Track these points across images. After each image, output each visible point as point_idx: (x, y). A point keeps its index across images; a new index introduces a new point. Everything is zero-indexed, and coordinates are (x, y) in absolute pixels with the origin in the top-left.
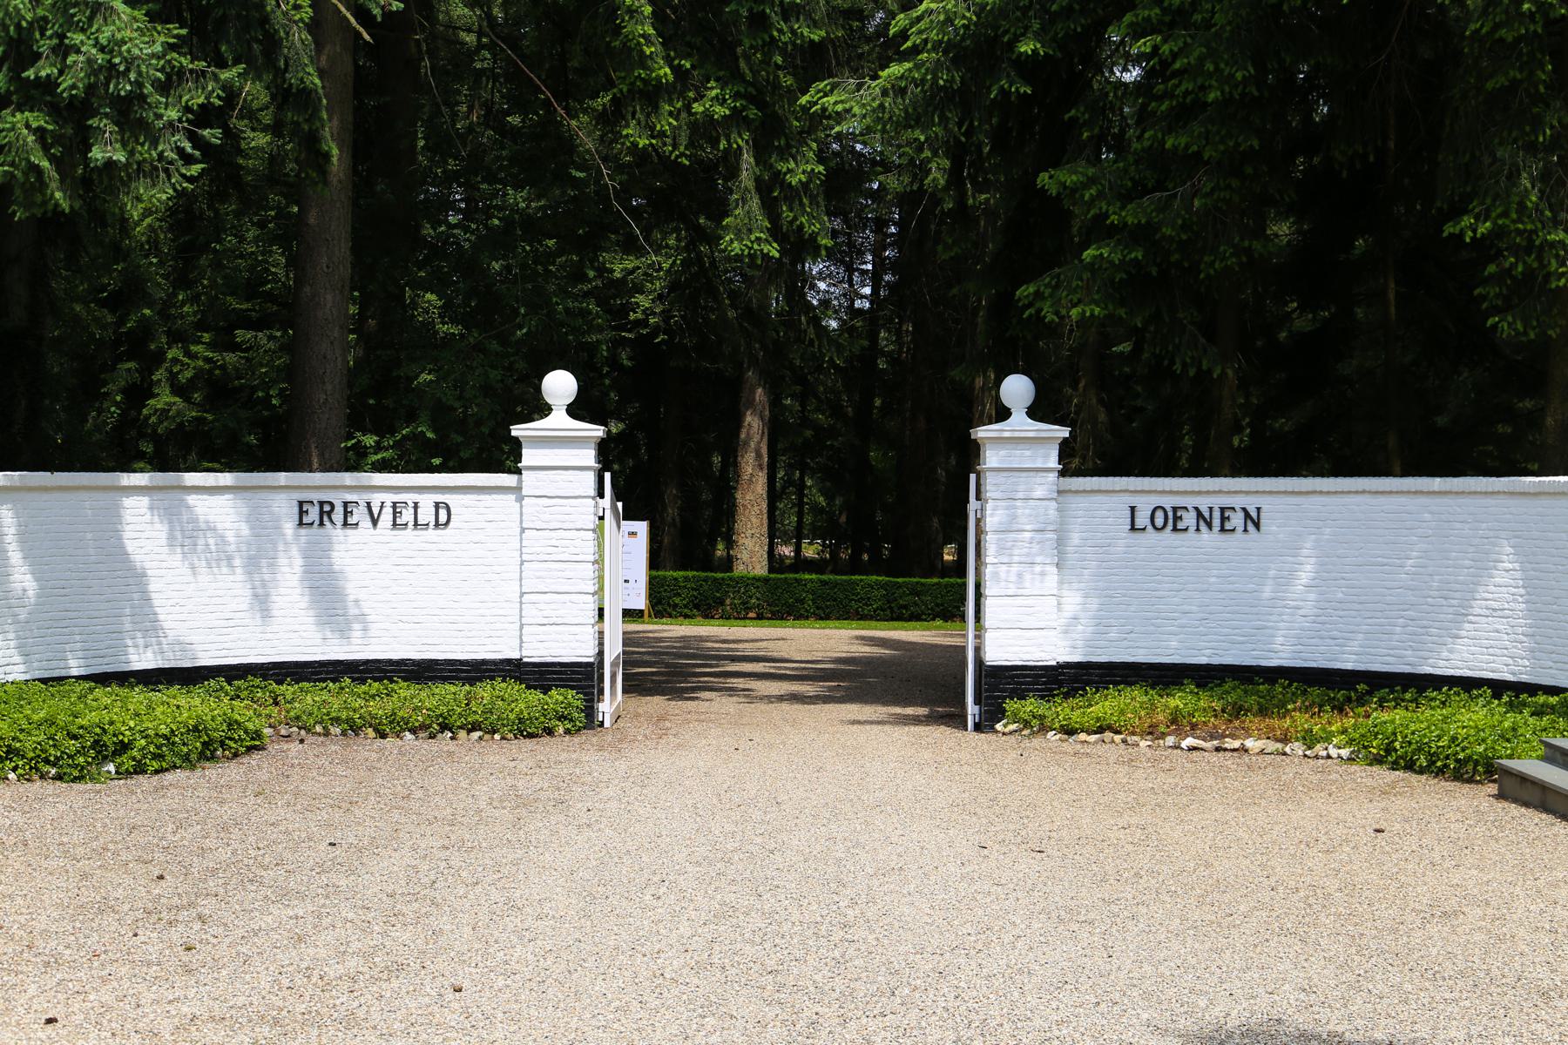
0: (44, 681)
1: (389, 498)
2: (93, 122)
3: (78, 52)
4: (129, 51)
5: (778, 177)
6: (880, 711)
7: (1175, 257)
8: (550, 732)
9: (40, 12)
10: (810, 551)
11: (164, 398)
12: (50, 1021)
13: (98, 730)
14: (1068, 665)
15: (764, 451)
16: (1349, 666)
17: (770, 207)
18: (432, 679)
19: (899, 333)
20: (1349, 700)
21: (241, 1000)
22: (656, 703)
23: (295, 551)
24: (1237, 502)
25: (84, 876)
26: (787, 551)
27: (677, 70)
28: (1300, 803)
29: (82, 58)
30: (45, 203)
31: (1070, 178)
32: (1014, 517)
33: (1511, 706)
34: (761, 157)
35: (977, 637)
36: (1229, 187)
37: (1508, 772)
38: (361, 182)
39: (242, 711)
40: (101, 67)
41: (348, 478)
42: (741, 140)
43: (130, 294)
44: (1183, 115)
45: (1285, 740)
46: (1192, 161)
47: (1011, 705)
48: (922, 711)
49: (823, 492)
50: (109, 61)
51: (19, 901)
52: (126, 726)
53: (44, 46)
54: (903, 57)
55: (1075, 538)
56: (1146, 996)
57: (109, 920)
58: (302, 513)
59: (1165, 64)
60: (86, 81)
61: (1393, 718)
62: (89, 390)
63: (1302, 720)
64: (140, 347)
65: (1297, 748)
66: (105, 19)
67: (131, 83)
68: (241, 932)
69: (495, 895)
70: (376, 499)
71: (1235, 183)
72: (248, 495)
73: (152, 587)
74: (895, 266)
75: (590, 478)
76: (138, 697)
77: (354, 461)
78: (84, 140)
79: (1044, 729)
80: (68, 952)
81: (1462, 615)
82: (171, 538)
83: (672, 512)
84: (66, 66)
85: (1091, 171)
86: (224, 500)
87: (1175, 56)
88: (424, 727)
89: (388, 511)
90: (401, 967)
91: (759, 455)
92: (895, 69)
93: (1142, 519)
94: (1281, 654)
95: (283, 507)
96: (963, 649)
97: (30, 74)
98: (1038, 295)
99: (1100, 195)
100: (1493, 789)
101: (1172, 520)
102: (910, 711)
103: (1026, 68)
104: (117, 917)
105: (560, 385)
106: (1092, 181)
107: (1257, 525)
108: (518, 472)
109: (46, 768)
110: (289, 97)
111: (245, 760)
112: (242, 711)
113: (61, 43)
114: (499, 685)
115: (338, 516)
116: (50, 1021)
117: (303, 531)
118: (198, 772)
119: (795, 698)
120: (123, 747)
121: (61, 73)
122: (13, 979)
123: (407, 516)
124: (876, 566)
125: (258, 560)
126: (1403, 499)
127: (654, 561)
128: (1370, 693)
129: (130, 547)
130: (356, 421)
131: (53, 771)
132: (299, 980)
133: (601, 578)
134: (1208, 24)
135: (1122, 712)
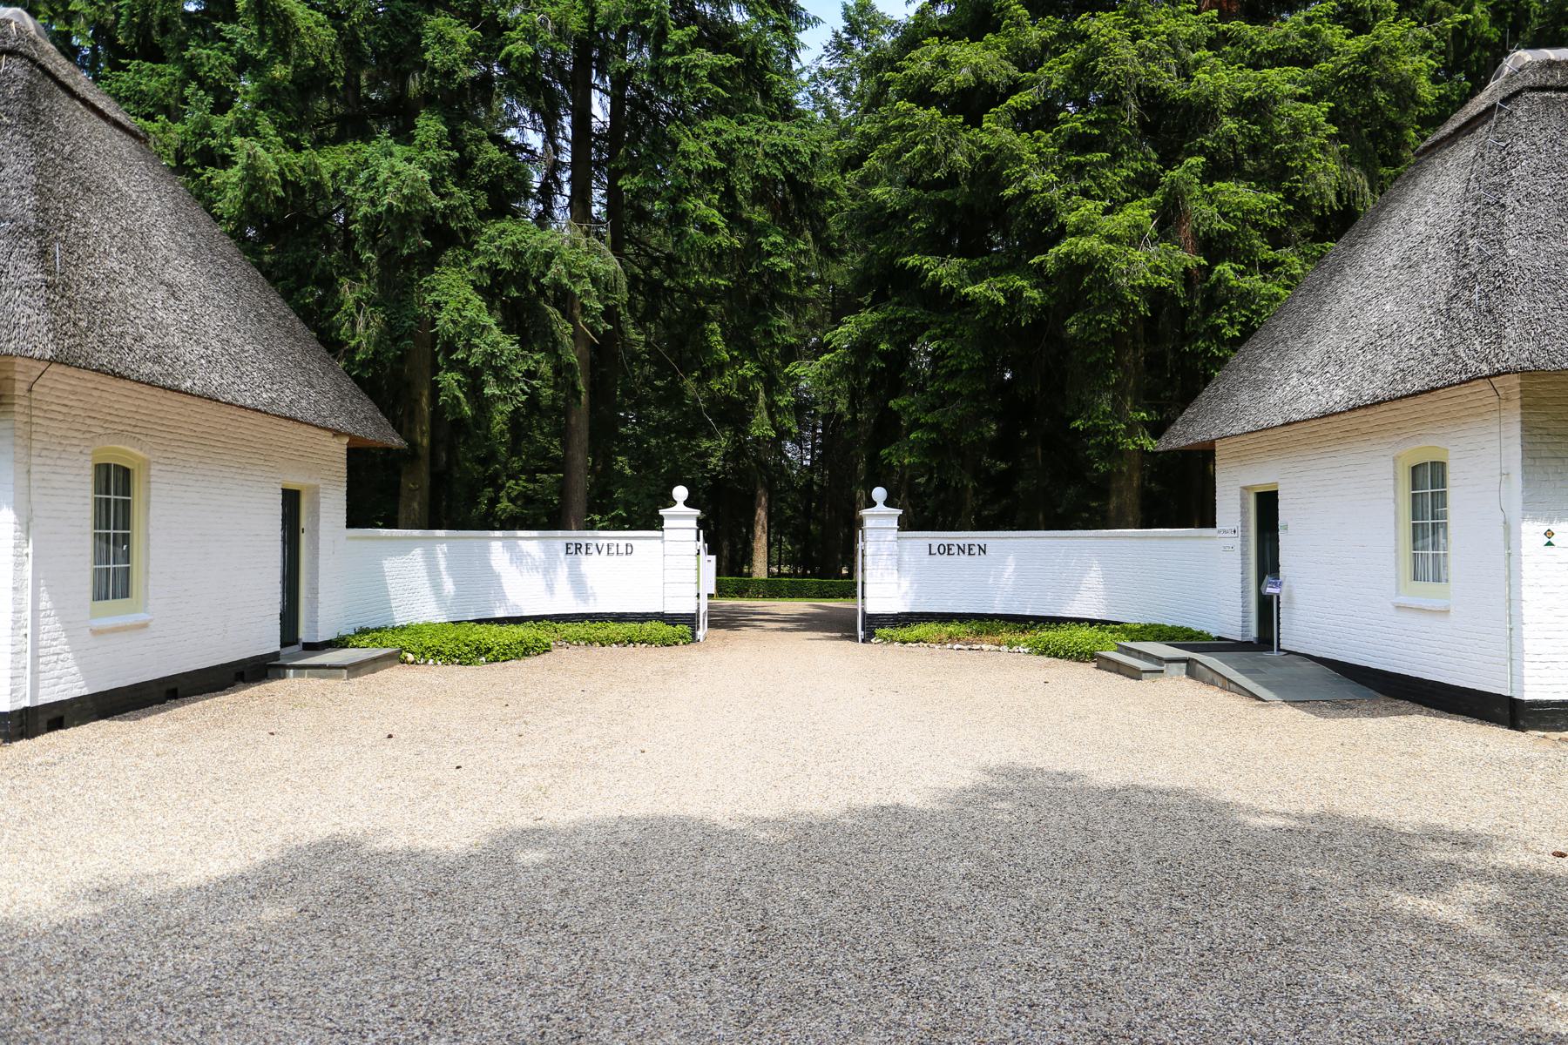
0: (453, 622)
1: (606, 542)
3: (477, 347)
5: (774, 403)
6: (820, 635)
7: (949, 437)
8: (676, 644)
9: (458, 330)
10: (785, 569)
11: (504, 504)
12: (458, 767)
14: (903, 614)
15: (766, 526)
16: (1027, 613)
17: (771, 416)
18: (625, 621)
19: (822, 475)
20: (1026, 628)
21: (545, 758)
22: (723, 632)
23: (564, 565)
24: (976, 542)
26: (775, 570)
27: (732, 356)
28: (1009, 671)
30: (460, 413)
31: (902, 403)
32: (879, 549)
33: (1100, 629)
34: (768, 392)
35: (863, 605)
36: (972, 406)
37: (1101, 657)
38: (593, 407)
39: (541, 635)
41: (588, 533)
42: (759, 386)
43: (492, 457)
44: (953, 374)
45: (999, 645)
46: (955, 395)
47: (878, 631)
48: (840, 635)
49: (790, 544)
52: (490, 641)
53: (460, 344)
54: (829, 352)
55: (906, 558)
56: (952, 752)
57: (484, 723)
58: (567, 548)
59: (944, 353)
61: (1047, 635)
62: (473, 501)
63: (1007, 637)
64: (494, 482)
65: (1005, 648)
68: (543, 729)
69: (657, 711)
70: (600, 542)
71: (975, 404)
72: (544, 540)
73: (503, 581)
74: (820, 447)
75: (694, 533)
76: (495, 628)
77: (591, 526)
79: (893, 641)
81: (1077, 590)
82: (511, 560)
83: (725, 552)
85: (912, 400)
86: (534, 542)
87: (948, 349)
88: (621, 642)
89: (605, 548)
90: (617, 743)
91: (763, 527)
92: (827, 357)
93: (934, 550)
94: (998, 608)
95: (560, 546)
96: (856, 610)
97: (454, 357)
98: (890, 454)
99: (916, 410)
100: (1094, 665)
101: (948, 550)
102: (833, 635)
103: (884, 356)
105: (680, 493)
106: (912, 404)
107: (985, 552)
108: (662, 530)
110: (562, 370)
111: (543, 656)
112: (541, 635)
114: (654, 623)
115: (584, 550)
116: (458, 767)
117: (568, 556)
118: (522, 661)
119: (782, 629)
120: (489, 650)
122: (441, 750)
123: (614, 550)
124: (813, 575)
125: (548, 569)
126: (1048, 540)
127: (718, 573)
128: (1035, 625)
129: (493, 563)
130: (591, 509)
132: (571, 749)
133: (698, 577)
134: (962, 336)
135: (927, 634)
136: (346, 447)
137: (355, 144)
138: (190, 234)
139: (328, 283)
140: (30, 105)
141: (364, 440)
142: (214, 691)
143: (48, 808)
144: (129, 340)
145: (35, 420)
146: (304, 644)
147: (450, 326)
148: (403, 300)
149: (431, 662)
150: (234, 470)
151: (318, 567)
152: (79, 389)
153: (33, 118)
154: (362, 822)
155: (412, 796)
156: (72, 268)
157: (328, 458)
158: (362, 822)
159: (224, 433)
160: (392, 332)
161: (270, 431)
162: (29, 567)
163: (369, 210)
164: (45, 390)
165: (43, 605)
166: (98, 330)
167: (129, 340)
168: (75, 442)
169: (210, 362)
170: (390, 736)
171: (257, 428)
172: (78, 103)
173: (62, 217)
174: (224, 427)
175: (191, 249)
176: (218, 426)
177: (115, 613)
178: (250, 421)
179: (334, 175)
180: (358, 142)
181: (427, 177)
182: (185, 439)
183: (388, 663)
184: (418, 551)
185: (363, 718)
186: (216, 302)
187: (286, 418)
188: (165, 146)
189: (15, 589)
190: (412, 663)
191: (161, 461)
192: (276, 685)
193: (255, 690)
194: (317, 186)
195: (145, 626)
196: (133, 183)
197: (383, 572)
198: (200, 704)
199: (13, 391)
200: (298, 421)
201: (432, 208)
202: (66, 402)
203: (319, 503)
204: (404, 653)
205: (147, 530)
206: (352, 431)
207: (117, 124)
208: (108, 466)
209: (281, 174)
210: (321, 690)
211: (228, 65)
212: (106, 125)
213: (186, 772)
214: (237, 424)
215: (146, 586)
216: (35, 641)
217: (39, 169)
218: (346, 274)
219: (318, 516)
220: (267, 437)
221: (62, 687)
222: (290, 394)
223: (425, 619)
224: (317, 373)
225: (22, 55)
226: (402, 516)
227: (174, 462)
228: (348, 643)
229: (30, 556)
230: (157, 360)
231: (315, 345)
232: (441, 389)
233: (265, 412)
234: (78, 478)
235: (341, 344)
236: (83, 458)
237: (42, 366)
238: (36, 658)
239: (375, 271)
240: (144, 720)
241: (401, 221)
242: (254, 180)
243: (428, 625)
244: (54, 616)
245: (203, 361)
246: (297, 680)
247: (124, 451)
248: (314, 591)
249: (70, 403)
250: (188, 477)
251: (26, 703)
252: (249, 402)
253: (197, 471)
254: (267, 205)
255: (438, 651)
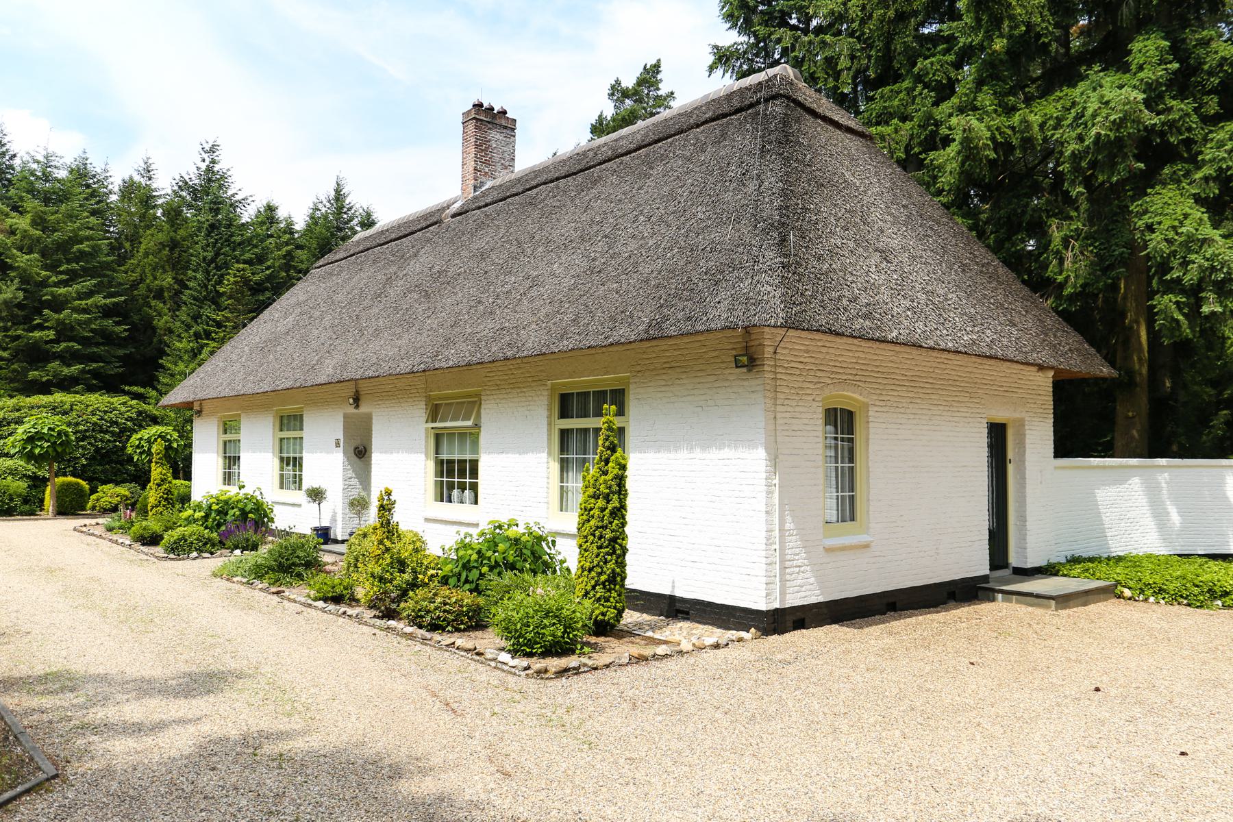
2: (1203, 295)
3: (1194, 263)
4: (1222, 258)
9: (1173, 248)
12: (1183, 754)
13: (1211, 584)
25: (1204, 663)
29: (1196, 265)
30: (1180, 335)
40: (1207, 268)
50: (1212, 265)
51: (1165, 672)
60: (1198, 276)
66: (1209, 246)
67: (1224, 273)
78: (1199, 302)
80: (1195, 708)
84: (1187, 271)
97: (1168, 277)
104: (1225, 691)
109: (1182, 600)
113: (1185, 260)
116: (1183, 754)
121: (1184, 274)
131: (1185, 602)
136: (1051, 380)
137: (1062, 91)
138: (903, 206)
139: (1038, 229)
140: (783, 131)
141: (1069, 371)
142: (929, 607)
143: (772, 709)
144: (845, 302)
145: (779, 376)
146: (1014, 568)
147: (1164, 245)
148: (1113, 229)
149: (1152, 599)
150: (941, 408)
151: (1025, 496)
152: (811, 348)
153: (786, 139)
154: (1052, 810)
155: (1120, 785)
156: (803, 250)
157: (1033, 392)
158: (1052, 810)
159: (932, 375)
160: (1103, 265)
161: (975, 370)
162: (776, 495)
163: (1077, 147)
164: (786, 351)
165: (787, 526)
166: (820, 297)
167: (845, 302)
168: (809, 391)
169: (915, 312)
170: (1097, 690)
171: (962, 369)
172: (819, 121)
173: (799, 211)
174: (931, 370)
175: (903, 219)
176: (926, 369)
177: (849, 536)
178: (955, 362)
179: (1042, 126)
180: (1065, 88)
181: (1141, 97)
182: (897, 383)
183: (1102, 596)
184: (1136, 480)
185: (1068, 660)
186: (924, 260)
187: (987, 357)
188: (897, 143)
189: (767, 512)
190: (1130, 599)
191: (877, 403)
192: (984, 608)
193: (964, 612)
194: (1028, 142)
195: (867, 546)
196: (857, 173)
197: (1096, 501)
198: (913, 620)
199: (764, 354)
200: (999, 359)
201: (1146, 128)
202: (802, 360)
203: (1025, 435)
204: (1119, 587)
205: (867, 462)
206: (1055, 364)
207: (849, 130)
208: (836, 409)
209: (993, 139)
210: (1027, 619)
211: (948, 64)
212: (840, 133)
213: (887, 693)
214: (943, 366)
215: (868, 511)
216: (782, 555)
217: (786, 179)
218: (1055, 215)
219: (1025, 447)
220: (972, 375)
221: (803, 594)
222: (989, 335)
223: (1145, 550)
224: (1020, 312)
225: (782, 96)
226: (1119, 444)
227: (889, 404)
228: (1058, 571)
229: (777, 486)
230: (867, 316)
231: (1018, 286)
232: (1157, 314)
233: (966, 353)
234: (812, 422)
235: (1050, 282)
236: (815, 404)
237: (782, 332)
238: (783, 568)
239: (1084, 206)
240: (866, 630)
241: (1109, 149)
242: (969, 150)
243: (1149, 556)
244: (796, 535)
245: (909, 313)
246: (1005, 605)
247: (848, 397)
248: (1022, 518)
249: (805, 360)
250: (900, 416)
251: (777, 605)
252: (950, 345)
253: (908, 411)
254: (981, 169)
255: (1161, 590)
